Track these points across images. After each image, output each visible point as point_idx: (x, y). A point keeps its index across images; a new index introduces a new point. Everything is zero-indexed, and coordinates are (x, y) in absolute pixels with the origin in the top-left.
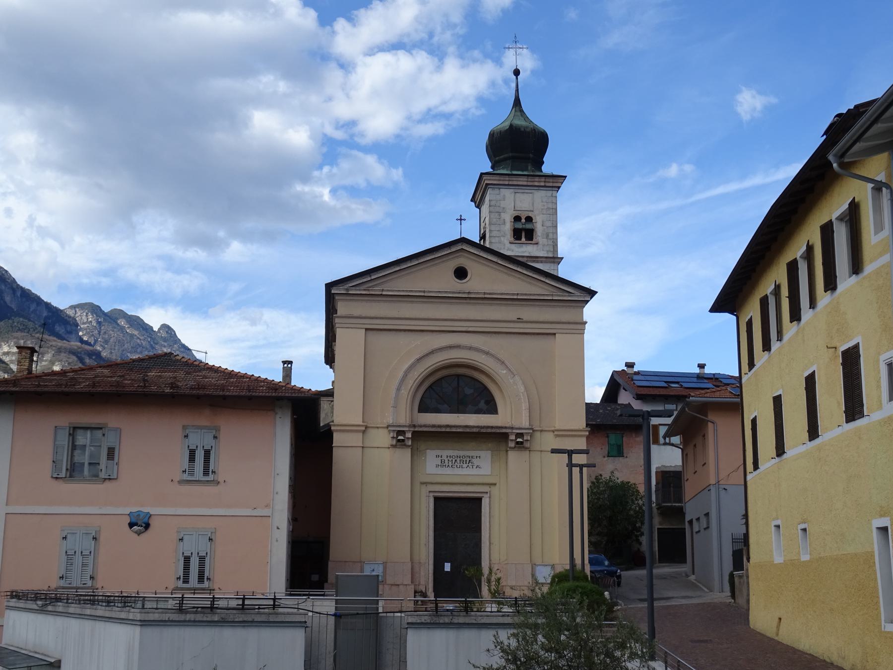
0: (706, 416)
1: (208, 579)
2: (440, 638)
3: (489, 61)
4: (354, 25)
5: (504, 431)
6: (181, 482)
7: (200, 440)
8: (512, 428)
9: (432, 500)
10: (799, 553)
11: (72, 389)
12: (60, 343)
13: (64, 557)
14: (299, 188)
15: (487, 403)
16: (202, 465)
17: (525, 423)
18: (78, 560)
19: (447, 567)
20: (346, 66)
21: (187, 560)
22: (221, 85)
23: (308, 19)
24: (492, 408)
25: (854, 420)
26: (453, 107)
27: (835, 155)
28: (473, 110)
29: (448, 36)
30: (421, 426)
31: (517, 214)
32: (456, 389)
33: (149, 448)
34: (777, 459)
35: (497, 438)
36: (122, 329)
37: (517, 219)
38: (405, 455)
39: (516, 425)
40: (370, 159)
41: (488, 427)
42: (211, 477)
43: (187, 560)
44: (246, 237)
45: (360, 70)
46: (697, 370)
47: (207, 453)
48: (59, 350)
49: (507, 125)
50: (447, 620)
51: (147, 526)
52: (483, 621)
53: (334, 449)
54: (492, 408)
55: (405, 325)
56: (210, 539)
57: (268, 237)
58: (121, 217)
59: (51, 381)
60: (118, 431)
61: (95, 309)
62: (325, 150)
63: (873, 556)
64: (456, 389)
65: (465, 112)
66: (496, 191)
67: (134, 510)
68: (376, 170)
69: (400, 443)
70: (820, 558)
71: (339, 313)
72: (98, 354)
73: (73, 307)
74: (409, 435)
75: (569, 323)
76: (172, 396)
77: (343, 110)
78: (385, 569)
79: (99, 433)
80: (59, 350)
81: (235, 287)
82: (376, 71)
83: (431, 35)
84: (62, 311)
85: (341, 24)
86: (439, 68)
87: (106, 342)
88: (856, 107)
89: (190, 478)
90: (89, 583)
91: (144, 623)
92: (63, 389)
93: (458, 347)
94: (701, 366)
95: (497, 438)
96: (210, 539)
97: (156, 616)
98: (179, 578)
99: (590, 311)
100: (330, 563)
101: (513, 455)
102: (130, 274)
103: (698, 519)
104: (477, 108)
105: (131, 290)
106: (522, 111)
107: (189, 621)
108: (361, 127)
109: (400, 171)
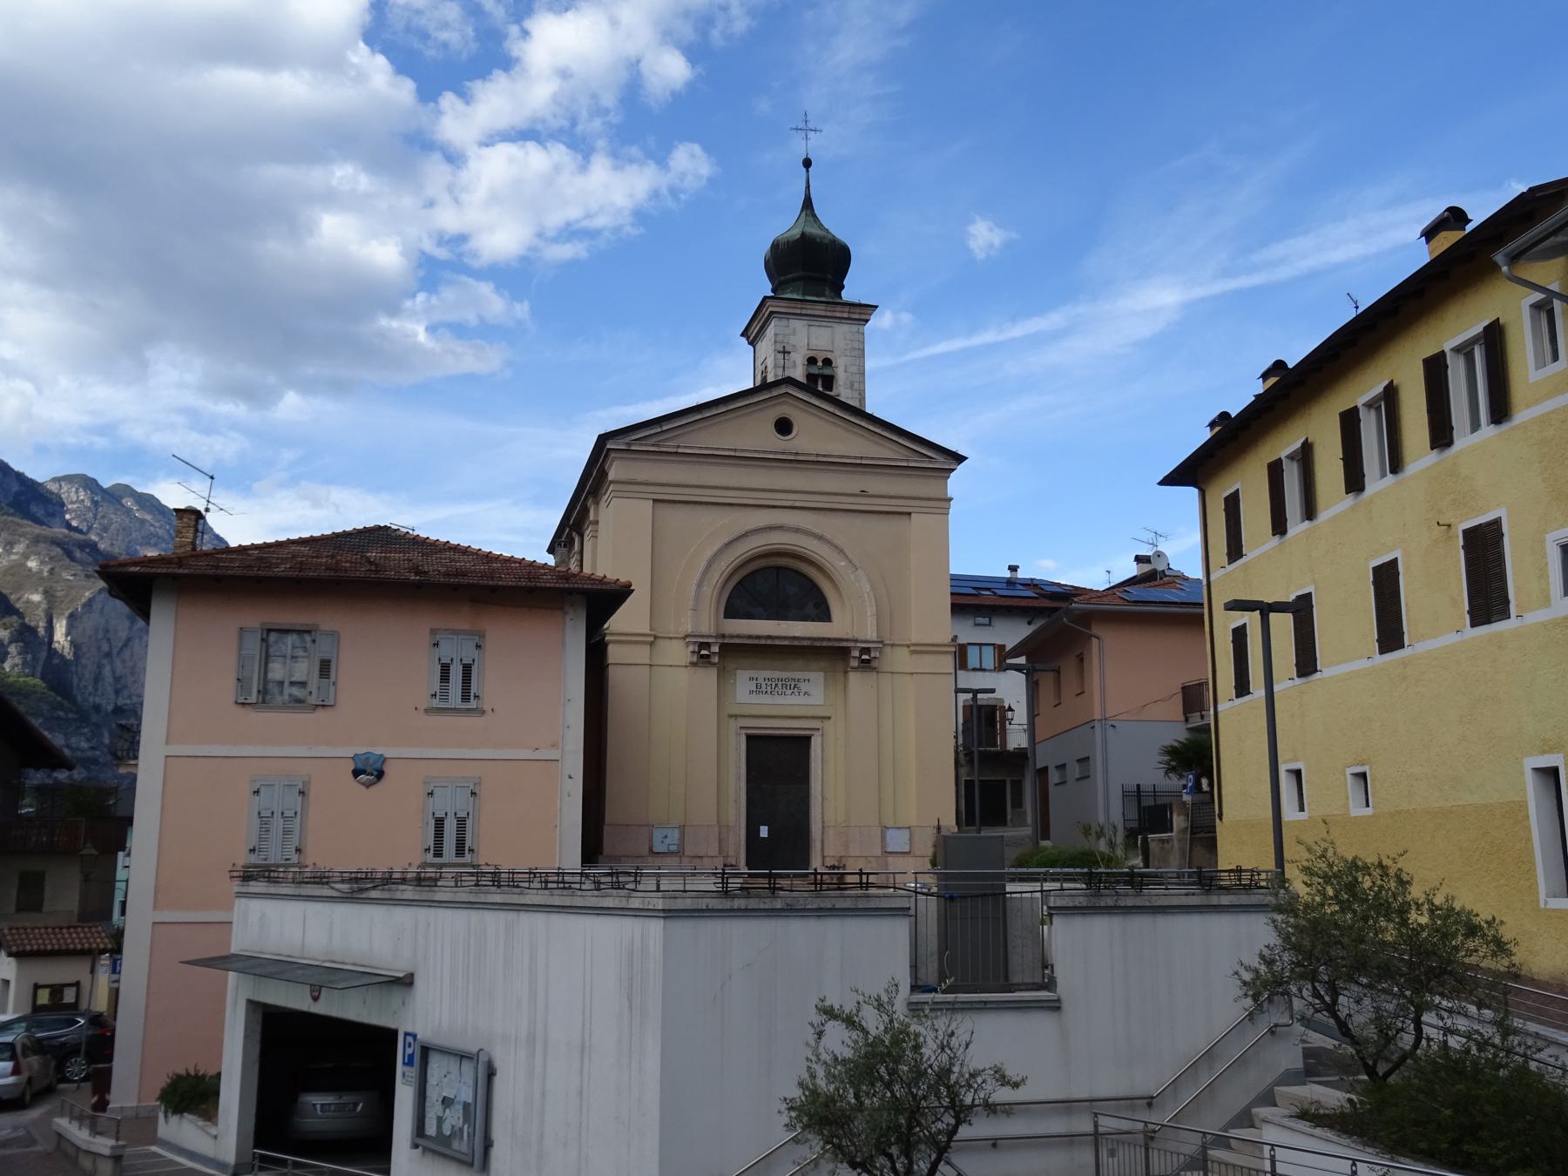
0: (1089, 628)
1: (471, 850)
2: (1101, 928)
3: (651, 162)
4: (468, 103)
5: (845, 644)
6: (427, 711)
7: (456, 650)
8: (856, 641)
9: (744, 739)
10: (1346, 806)
11: (270, 574)
12: (38, 530)
13: (256, 821)
14: (384, 322)
15: (817, 606)
16: (460, 685)
17: (871, 634)
18: (277, 824)
19: (764, 832)
20: (454, 158)
21: (439, 823)
22: (275, 174)
23: (404, 91)
24: (824, 615)
25: (1488, 621)
26: (600, 222)
27: (1507, 255)
28: (628, 229)
29: (597, 124)
30: (732, 637)
31: (811, 354)
32: (775, 586)
33: (383, 666)
34: (1298, 681)
35: (835, 656)
36: (129, 511)
37: (812, 361)
38: (709, 677)
39: (861, 637)
40: (485, 289)
41: (823, 639)
42: (473, 704)
43: (439, 823)
44: (307, 387)
45: (473, 164)
46: (1008, 574)
47: (467, 670)
48: (37, 540)
49: (796, 233)
50: (1110, 902)
51: (380, 775)
52: (1160, 903)
53: (611, 670)
54: (824, 615)
55: (731, 497)
56: (473, 793)
57: (338, 388)
58: (125, 352)
59: (231, 560)
60: (334, 635)
61: (89, 484)
62: (422, 273)
63: (1523, 805)
64: (775, 586)
65: (617, 230)
66: (784, 322)
67: (361, 750)
68: (494, 303)
69: (702, 660)
70: (1399, 812)
71: (611, 476)
72: (93, 546)
73: (55, 480)
74: (715, 649)
75: (929, 499)
76: (418, 586)
77: (448, 219)
78: (683, 834)
79: (308, 638)
80: (37, 540)
81: (288, 455)
82: (495, 167)
83: (574, 122)
84: (40, 484)
85: (448, 100)
86: (584, 168)
87: (105, 529)
88: (1530, 189)
89: (442, 705)
90: (295, 858)
91: (668, 914)
92: (255, 572)
93: (780, 528)
94: (1013, 569)
95: (835, 656)
96: (473, 793)
97: (687, 903)
98: (428, 850)
99: (956, 483)
100: (606, 828)
101: (854, 678)
102: (137, 434)
103: (1062, 767)
104: (633, 225)
105: (138, 456)
106: (814, 216)
107: (739, 910)
108: (473, 244)
109: (526, 306)
